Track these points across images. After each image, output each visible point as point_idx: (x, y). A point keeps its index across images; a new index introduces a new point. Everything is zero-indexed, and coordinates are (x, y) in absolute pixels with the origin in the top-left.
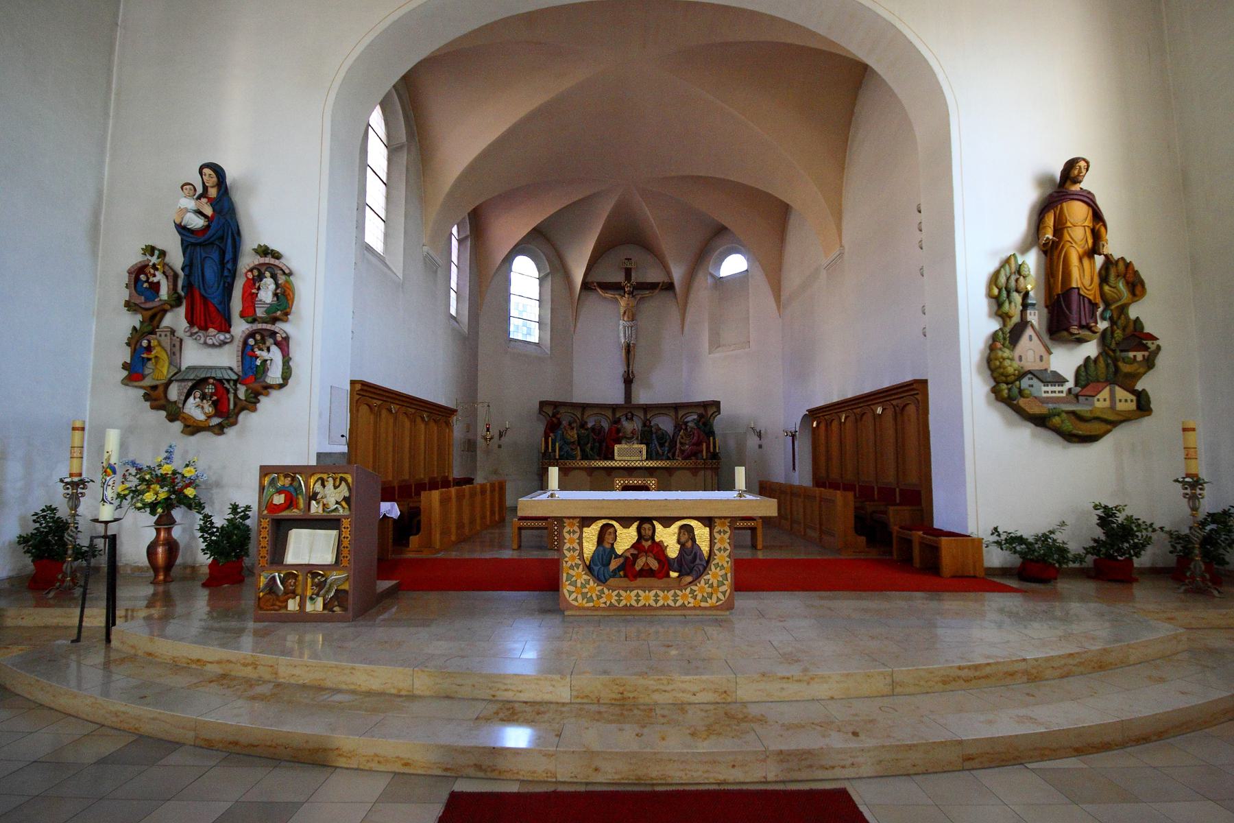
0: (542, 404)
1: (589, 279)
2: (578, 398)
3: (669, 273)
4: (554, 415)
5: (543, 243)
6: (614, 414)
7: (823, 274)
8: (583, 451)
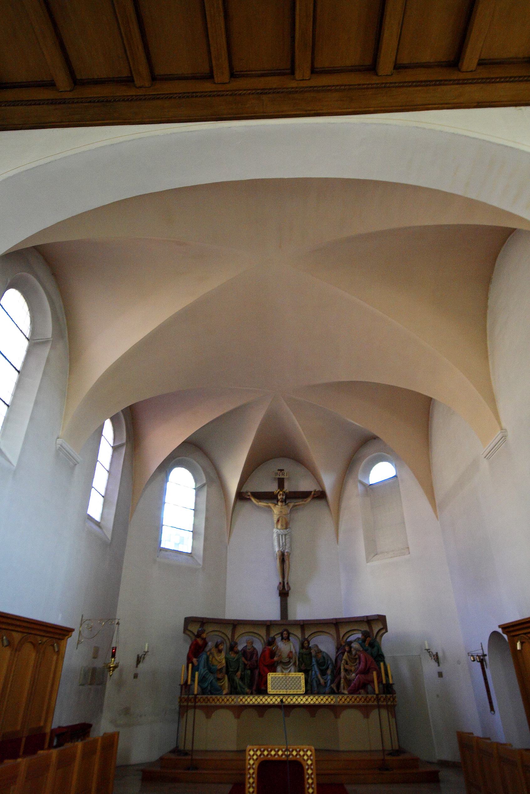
0: (189, 621)
1: (244, 490)
2: (231, 614)
3: (319, 481)
4: (199, 635)
5: (196, 452)
6: (268, 633)
7: (484, 464)
8: (231, 680)
